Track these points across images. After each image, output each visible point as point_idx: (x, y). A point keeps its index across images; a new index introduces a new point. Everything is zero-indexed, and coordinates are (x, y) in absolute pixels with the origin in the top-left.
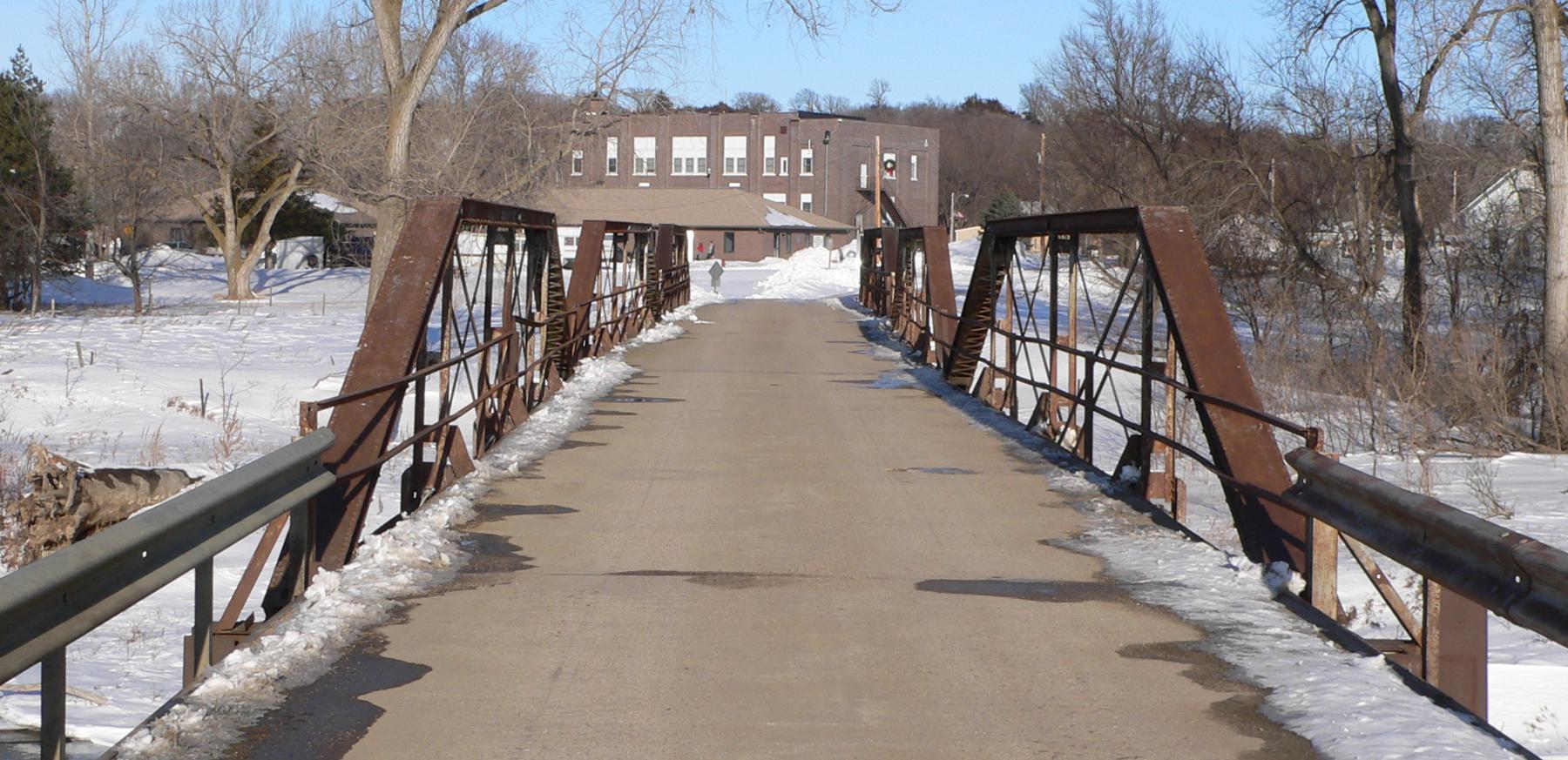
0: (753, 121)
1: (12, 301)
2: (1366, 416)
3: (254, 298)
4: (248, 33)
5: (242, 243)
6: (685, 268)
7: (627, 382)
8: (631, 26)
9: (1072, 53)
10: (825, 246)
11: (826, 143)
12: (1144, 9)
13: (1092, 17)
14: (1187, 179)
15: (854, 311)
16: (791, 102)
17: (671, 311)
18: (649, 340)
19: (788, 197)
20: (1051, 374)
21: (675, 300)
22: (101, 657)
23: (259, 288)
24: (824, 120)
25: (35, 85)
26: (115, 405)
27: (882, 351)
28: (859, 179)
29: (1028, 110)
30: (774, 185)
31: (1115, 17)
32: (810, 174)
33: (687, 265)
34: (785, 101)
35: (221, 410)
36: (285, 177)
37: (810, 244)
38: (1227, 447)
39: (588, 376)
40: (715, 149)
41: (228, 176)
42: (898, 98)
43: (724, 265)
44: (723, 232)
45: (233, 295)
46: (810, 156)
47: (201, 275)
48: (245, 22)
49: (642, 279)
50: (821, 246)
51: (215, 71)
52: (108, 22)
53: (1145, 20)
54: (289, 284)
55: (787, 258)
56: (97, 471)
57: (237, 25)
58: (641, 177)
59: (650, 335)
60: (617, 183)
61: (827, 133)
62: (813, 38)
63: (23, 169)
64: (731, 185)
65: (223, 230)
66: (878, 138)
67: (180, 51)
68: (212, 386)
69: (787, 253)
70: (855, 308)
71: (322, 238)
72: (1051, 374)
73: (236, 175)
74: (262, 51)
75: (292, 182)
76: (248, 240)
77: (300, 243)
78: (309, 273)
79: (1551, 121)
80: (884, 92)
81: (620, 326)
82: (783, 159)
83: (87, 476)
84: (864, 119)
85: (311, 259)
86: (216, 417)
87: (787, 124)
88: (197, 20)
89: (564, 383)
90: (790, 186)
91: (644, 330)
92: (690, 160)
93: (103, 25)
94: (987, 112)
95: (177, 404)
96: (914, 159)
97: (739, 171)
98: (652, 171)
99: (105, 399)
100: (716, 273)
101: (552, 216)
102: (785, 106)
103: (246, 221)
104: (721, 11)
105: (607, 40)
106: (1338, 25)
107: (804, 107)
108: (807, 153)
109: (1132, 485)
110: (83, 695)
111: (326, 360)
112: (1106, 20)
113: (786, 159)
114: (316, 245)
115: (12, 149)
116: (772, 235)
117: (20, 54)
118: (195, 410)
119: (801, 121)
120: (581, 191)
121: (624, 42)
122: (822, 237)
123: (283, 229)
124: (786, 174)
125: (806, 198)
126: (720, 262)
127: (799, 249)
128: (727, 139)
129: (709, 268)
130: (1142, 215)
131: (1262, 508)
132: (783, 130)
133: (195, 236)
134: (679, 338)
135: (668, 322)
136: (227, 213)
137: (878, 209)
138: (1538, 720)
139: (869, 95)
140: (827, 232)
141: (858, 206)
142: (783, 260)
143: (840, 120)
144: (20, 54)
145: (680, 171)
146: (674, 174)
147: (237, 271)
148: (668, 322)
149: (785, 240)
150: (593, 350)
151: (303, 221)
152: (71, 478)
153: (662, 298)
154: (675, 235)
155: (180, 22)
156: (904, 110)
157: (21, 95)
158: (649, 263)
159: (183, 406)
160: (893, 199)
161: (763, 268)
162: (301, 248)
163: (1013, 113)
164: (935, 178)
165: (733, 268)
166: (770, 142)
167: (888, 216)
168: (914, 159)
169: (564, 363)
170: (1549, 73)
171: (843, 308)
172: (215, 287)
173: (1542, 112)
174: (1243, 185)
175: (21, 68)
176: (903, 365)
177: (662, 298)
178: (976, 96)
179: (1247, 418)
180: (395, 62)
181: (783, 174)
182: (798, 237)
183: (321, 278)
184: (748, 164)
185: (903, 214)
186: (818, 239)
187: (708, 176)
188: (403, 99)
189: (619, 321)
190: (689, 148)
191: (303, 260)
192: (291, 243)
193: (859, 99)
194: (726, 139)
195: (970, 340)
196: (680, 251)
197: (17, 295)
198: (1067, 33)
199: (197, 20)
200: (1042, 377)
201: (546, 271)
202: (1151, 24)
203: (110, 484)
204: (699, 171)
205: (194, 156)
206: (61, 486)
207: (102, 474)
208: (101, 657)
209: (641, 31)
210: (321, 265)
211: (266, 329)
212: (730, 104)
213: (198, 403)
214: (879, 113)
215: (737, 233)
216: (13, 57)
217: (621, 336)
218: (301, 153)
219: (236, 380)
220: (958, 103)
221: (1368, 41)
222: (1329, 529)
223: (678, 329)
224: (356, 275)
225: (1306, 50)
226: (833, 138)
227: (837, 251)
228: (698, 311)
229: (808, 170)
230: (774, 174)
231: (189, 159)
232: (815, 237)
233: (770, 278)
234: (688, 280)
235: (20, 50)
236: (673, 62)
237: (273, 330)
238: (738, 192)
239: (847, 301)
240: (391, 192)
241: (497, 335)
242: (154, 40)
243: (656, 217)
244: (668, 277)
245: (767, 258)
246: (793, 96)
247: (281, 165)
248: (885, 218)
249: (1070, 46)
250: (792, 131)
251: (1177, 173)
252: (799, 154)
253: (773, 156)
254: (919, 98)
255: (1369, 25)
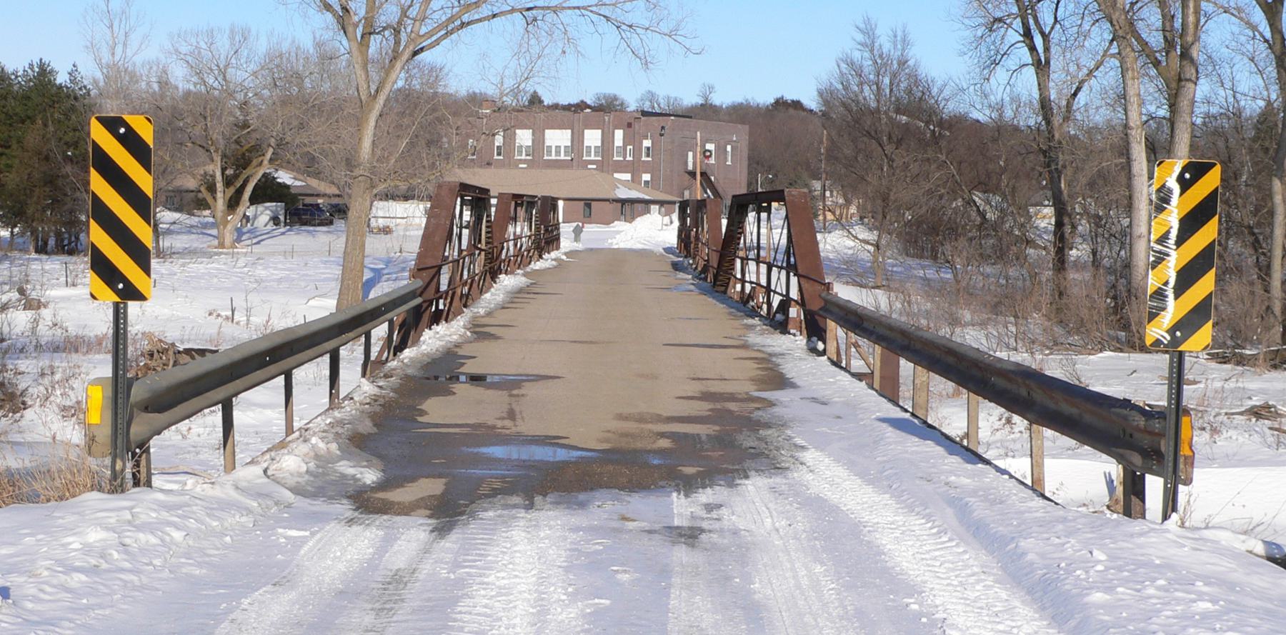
0: (606, 118)
1: (66, 248)
2: (1013, 329)
3: (237, 248)
4: (235, 53)
5: (228, 207)
6: (557, 226)
7: (528, 286)
8: (523, 62)
9: (844, 71)
10: (659, 213)
11: (661, 135)
12: (899, 38)
13: (859, 44)
14: (906, 166)
15: (671, 256)
16: (637, 101)
17: (549, 253)
18: (537, 268)
19: (632, 176)
20: (758, 277)
21: (551, 246)
22: (201, 457)
23: (239, 240)
24: (661, 118)
25: (84, 91)
26: (173, 315)
27: (681, 275)
28: (686, 163)
29: (823, 109)
30: (621, 167)
31: (876, 44)
32: (650, 159)
33: (559, 224)
34: (632, 100)
35: (245, 318)
36: (260, 159)
37: (649, 212)
38: (806, 296)
39: (506, 283)
40: (577, 140)
41: (219, 158)
42: (723, 98)
43: (583, 227)
44: (583, 202)
45: (222, 245)
46: (650, 145)
47: (195, 231)
48: (232, 44)
49: (531, 230)
50: (657, 213)
51: (211, 80)
52: (129, 42)
53: (899, 46)
54: (260, 238)
55: (630, 222)
56: (185, 349)
57: (227, 46)
58: (521, 160)
59: (538, 265)
60: (501, 164)
61: (663, 128)
62: (645, 71)
63: (77, 152)
64: (590, 166)
65: (215, 198)
66: (698, 134)
67: (185, 66)
68: (239, 303)
69: (631, 219)
70: (673, 254)
71: (283, 204)
72: (758, 277)
73: (224, 156)
74: (245, 66)
75: (266, 162)
76: (233, 204)
77: (267, 208)
78: (274, 230)
79: (1133, 132)
80: (710, 93)
81: (519, 259)
82: (629, 147)
83: (179, 352)
84: (691, 117)
85: (275, 220)
86: (242, 323)
87: (632, 121)
88: (198, 43)
89: (465, 309)
90: (634, 168)
91: (533, 263)
92: (558, 148)
93: (125, 45)
94: (791, 111)
95: (215, 314)
96: (729, 148)
97: (595, 156)
98: (529, 155)
99: (166, 310)
100: (578, 232)
101: (488, 190)
102: (632, 106)
103: (231, 191)
104: (583, 52)
105: (507, 72)
106: (1011, 62)
107: (647, 107)
108: (647, 143)
109: (781, 323)
110: (200, 474)
111: (312, 286)
112: (869, 45)
113: (631, 147)
114: (279, 209)
115: (69, 137)
116: (620, 205)
117: (74, 69)
118: (227, 318)
119: (643, 118)
120: (476, 170)
121: (520, 74)
122: (657, 207)
123: (256, 199)
124: (631, 159)
125: (647, 177)
126: (580, 224)
127: (640, 216)
128: (586, 132)
129: (572, 229)
130: (786, 193)
131: (816, 320)
132: (629, 125)
133: (192, 202)
134: (555, 267)
135: (547, 260)
136: (218, 185)
137: (698, 182)
138: (1057, 489)
139: (698, 96)
140: (661, 203)
141: (686, 183)
142: (628, 224)
143: (672, 118)
144: (74, 69)
145: (551, 155)
146: (546, 158)
147: (225, 227)
148: (547, 260)
149: (629, 208)
150: (503, 271)
151: (269, 192)
152: (171, 353)
153: (543, 244)
154: (550, 204)
155: (185, 44)
156: (727, 108)
157: (76, 98)
158: (536, 221)
159: (219, 315)
160: (713, 178)
161: (612, 229)
162: (268, 212)
163: (811, 111)
164: (745, 163)
165: (591, 229)
166: (619, 135)
167: (708, 191)
168: (729, 148)
169: (493, 272)
170: (1132, 100)
171: (664, 253)
172: (205, 240)
173: (1126, 126)
174: (942, 172)
175: (75, 79)
176: (692, 281)
177: (543, 244)
178: (783, 97)
179: (816, 284)
180: (365, 86)
181: (629, 158)
182: (639, 207)
183: (283, 234)
184: (603, 150)
185: (720, 190)
186: (654, 208)
187: (572, 160)
188: (370, 111)
189: (518, 256)
190: (558, 138)
191: (270, 220)
192: (260, 208)
193: (690, 98)
194: (586, 131)
195: (726, 264)
196: (554, 213)
197: (70, 243)
198: (841, 56)
199: (198, 43)
200: (754, 279)
201: (484, 221)
202: (903, 50)
203: (193, 358)
204: (565, 156)
205: (193, 143)
206: (164, 358)
207: (188, 352)
208: (201, 457)
209: (530, 68)
210: (282, 224)
211: (260, 268)
212: (589, 102)
213: (229, 313)
214: (706, 112)
215: (593, 203)
216: (70, 71)
217: (519, 265)
218: (273, 142)
219: (254, 299)
220: (768, 103)
221: (1030, 72)
222: (833, 323)
223: (554, 263)
224: (308, 232)
225: (988, 80)
226: (667, 131)
227: (668, 217)
228: (566, 254)
229: (648, 155)
230: (622, 159)
231: (189, 144)
232: (652, 207)
233: (618, 236)
234: (559, 234)
235: (74, 66)
236: (551, 89)
237: (265, 269)
238: (594, 172)
239: (668, 250)
240: (361, 172)
241: (465, 253)
242: (166, 58)
243: (540, 191)
244: (546, 230)
245: (616, 222)
246: (639, 97)
247: (257, 149)
248: (706, 193)
249: (843, 66)
250: (636, 126)
251: (898, 162)
252: (641, 143)
253: (621, 145)
254: (739, 99)
255: (1031, 62)
